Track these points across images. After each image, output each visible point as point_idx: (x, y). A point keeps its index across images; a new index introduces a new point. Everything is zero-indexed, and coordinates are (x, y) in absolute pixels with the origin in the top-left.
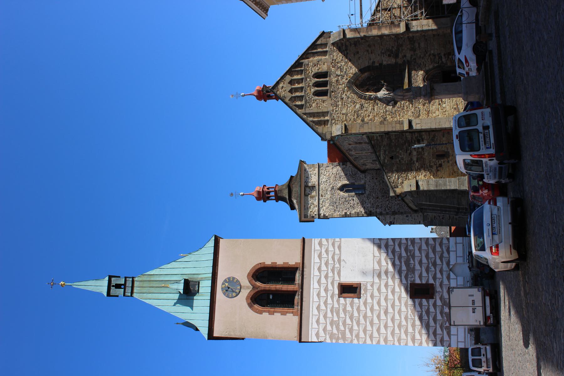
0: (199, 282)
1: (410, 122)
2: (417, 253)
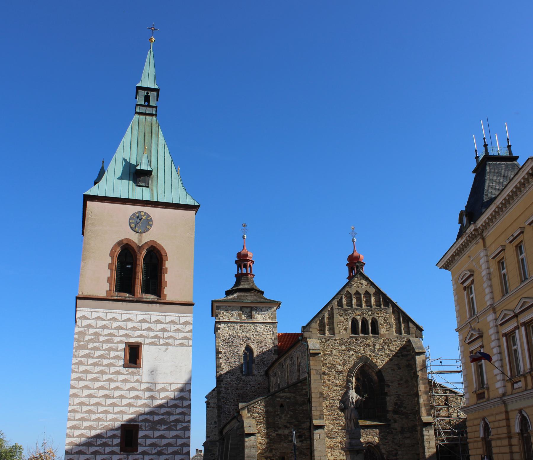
0: (148, 187)
1: (321, 427)
2: (173, 433)
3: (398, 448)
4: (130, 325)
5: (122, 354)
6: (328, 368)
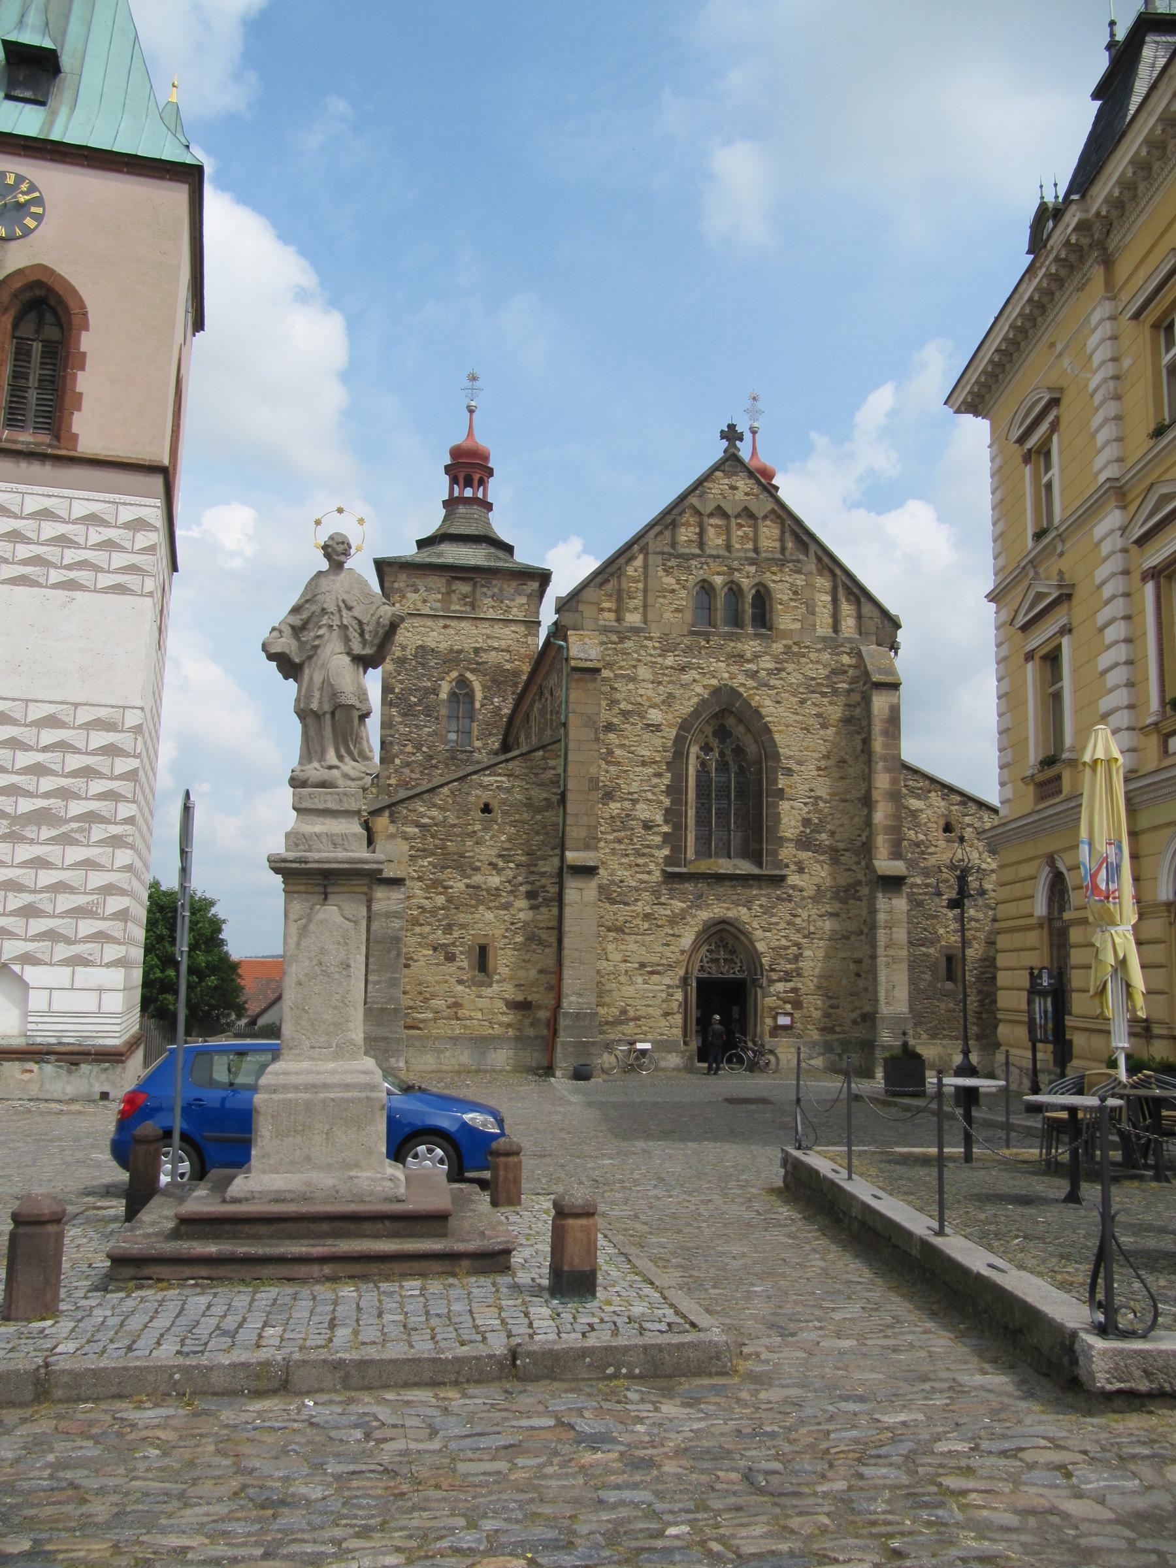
0: (42, 103)
1: (588, 871)
2: (75, 854)
6: (625, 714)
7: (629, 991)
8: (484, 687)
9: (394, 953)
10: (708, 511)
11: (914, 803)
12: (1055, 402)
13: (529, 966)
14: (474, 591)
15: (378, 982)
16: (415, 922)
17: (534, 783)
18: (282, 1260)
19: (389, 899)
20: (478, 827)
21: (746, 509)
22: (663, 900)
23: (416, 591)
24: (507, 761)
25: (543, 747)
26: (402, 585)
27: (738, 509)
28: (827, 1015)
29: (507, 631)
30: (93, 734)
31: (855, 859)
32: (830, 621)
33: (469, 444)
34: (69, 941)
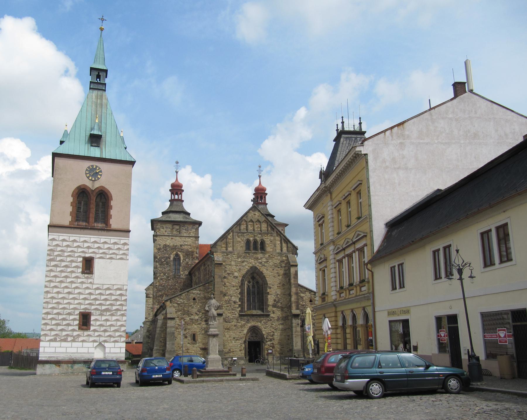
0: (99, 147)
2: (114, 318)
3: (274, 331)
4: (86, 245)
5: (80, 265)
6: (228, 274)
7: (231, 345)
8: (183, 256)
9: (173, 336)
10: (248, 221)
11: (302, 295)
12: (323, 217)
13: (206, 339)
14: (180, 228)
15: (169, 344)
16: (177, 328)
17: (206, 292)
18: (214, 375)
19: (171, 323)
20: (192, 304)
21: (258, 220)
22: (239, 321)
23: (163, 228)
24: (199, 287)
25: (208, 283)
26: (159, 227)
27: (256, 220)
28: (281, 350)
29: (190, 240)
30: (117, 291)
31: (287, 310)
32: (280, 248)
33: (176, 183)
34: (114, 337)
